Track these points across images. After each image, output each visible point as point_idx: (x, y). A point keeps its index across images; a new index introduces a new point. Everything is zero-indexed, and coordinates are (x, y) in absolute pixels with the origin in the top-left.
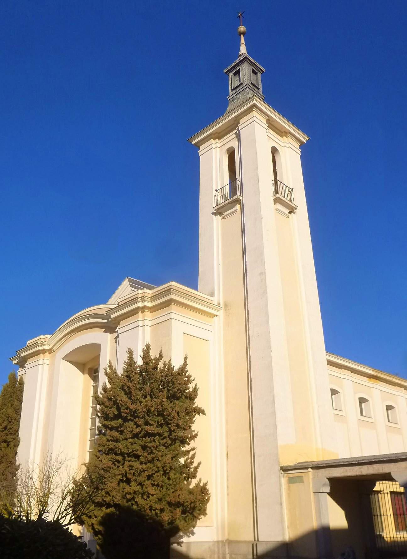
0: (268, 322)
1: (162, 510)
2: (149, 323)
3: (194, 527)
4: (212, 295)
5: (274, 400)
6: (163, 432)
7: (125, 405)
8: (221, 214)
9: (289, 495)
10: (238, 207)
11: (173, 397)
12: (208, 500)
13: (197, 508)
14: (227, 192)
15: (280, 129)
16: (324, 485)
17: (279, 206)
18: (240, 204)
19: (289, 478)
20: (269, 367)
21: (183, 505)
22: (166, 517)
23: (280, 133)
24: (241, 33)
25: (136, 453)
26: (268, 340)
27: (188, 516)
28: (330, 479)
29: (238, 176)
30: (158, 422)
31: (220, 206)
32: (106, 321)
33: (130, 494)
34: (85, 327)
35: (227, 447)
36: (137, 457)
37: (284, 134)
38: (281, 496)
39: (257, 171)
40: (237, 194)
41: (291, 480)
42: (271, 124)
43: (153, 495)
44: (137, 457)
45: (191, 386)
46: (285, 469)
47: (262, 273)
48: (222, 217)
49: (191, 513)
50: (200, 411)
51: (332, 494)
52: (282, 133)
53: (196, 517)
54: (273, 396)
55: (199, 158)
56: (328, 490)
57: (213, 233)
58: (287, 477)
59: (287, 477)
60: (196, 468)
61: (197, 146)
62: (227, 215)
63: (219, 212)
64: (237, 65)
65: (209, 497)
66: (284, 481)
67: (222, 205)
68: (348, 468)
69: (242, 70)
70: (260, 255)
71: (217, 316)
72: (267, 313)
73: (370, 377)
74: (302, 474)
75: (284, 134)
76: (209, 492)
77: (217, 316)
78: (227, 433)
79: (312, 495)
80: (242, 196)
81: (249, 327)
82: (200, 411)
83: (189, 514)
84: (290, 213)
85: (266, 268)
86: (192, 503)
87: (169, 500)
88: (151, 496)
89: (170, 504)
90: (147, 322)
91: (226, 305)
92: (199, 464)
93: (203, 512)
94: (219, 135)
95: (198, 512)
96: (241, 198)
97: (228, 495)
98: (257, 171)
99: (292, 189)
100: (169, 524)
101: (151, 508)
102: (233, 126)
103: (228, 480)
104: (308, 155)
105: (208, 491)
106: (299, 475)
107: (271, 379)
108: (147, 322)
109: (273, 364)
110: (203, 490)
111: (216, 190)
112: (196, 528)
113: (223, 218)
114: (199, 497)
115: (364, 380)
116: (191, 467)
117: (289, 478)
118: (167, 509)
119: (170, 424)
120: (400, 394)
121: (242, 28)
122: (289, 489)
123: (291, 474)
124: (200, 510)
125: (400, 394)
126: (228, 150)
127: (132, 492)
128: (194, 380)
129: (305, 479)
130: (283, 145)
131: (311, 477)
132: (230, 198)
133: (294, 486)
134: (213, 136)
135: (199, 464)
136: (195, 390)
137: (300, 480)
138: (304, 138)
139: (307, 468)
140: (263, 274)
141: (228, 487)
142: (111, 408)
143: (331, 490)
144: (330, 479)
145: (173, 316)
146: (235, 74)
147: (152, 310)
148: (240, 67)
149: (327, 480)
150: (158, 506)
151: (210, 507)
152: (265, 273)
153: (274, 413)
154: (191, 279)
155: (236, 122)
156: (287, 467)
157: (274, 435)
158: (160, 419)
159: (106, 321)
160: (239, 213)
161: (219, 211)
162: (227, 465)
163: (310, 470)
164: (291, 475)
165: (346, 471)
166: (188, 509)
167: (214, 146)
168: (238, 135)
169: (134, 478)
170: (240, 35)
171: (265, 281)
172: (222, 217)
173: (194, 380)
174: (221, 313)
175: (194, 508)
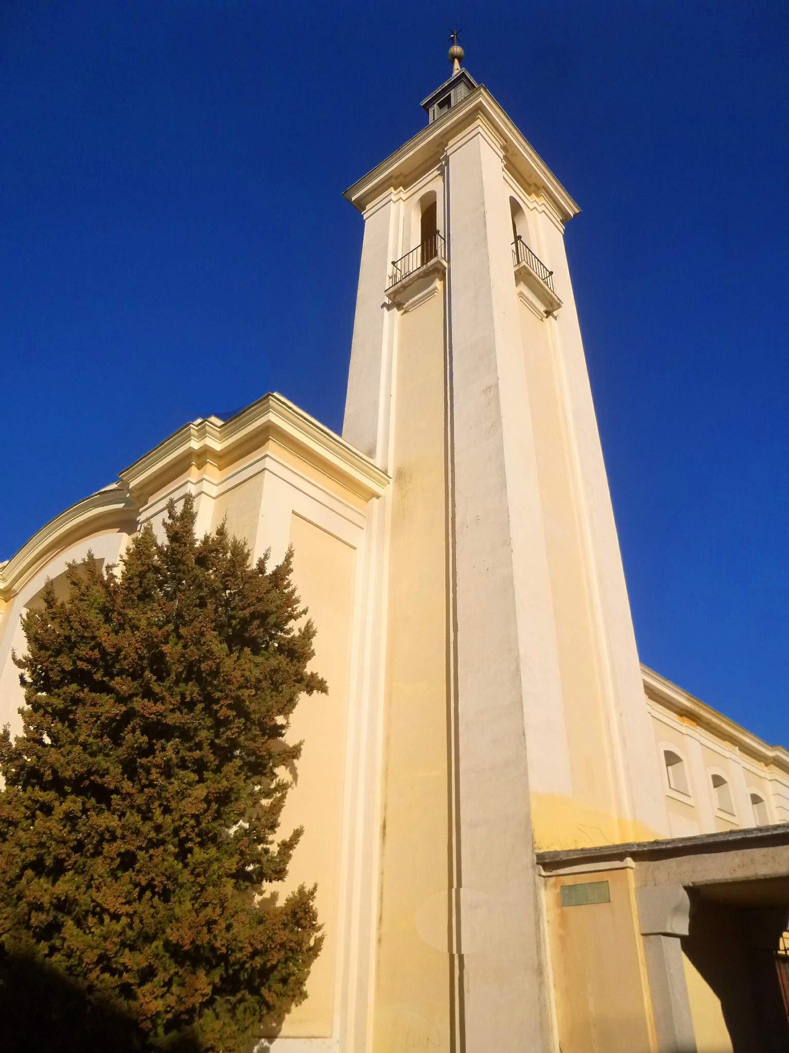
0: (503, 485)
1: (147, 974)
2: (214, 491)
3: (271, 1037)
4: (371, 453)
5: (518, 669)
6: (196, 729)
7: (94, 638)
8: (399, 306)
9: (563, 941)
10: (438, 284)
11: (239, 638)
12: (314, 951)
13: (276, 975)
14: (415, 262)
15: (526, 175)
16: (677, 910)
17: (523, 288)
18: (443, 278)
19: (563, 887)
20: (507, 587)
21: (224, 958)
22: (152, 1001)
23: (527, 186)
24: (454, 57)
25: (99, 780)
26: (505, 526)
27: (241, 1000)
28: (693, 891)
29: (440, 225)
30: (183, 696)
31: (399, 284)
32: (121, 506)
33: (39, 908)
34: (83, 532)
35: (385, 807)
36: (103, 795)
37: (533, 188)
38: (539, 944)
39: (477, 277)
40: (436, 254)
41: (569, 897)
42: (512, 165)
43: (116, 917)
44: (103, 795)
45: (295, 627)
46: (550, 863)
47: (490, 388)
48: (402, 311)
49: (255, 991)
50: (315, 685)
51: (689, 945)
52: (530, 185)
53: (270, 1008)
54: (517, 658)
55: (363, 222)
56: (682, 926)
57: (384, 346)
58: (555, 885)
59: (555, 885)
60: (286, 847)
61: (360, 206)
62: (413, 304)
63: (400, 297)
64: (445, 91)
65: (319, 941)
66: (547, 897)
67: (404, 281)
68: (758, 853)
69: (456, 95)
70: (486, 353)
71: (378, 497)
72: (502, 467)
73: (684, 713)
74: (604, 876)
75: (533, 188)
76: (319, 921)
77: (378, 497)
78: (386, 770)
79: (639, 941)
80: (449, 262)
81: (454, 506)
82: (315, 685)
83: (245, 992)
84: (548, 313)
85: (500, 377)
86: (255, 953)
87: (173, 938)
88: (107, 918)
89: (174, 951)
90: (206, 486)
91: (401, 474)
92: (297, 834)
93: (294, 990)
94: (404, 180)
95: (278, 987)
96: (445, 264)
97: (379, 941)
98: (477, 277)
99: (551, 273)
100: (168, 1027)
101: (105, 962)
102: (436, 159)
103: (381, 899)
104: (576, 236)
105: (314, 917)
106: (595, 878)
107: (511, 618)
108: (206, 486)
109: (516, 582)
110: (301, 913)
111: (394, 263)
112: (277, 1041)
113: (406, 312)
114: (283, 935)
115: (671, 718)
116: (270, 838)
117: (563, 887)
118: (168, 968)
119: (217, 701)
120: (733, 757)
121: (457, 49)
122: (563, 921)
123: (570, 876)
124: (284, 981)
125: (733, 757)
126: (422, 200)
127: (46, 899)
128: (305, 612)
129: (614, 891)
130: (531, 206)
131: (633, 885)
132: (423, 264)
133: (577, 914)
134: (393, 181)
135: (297, 834)
136: (308, 633)
137: (599, 894)
138: (572, 209)
139: (620, 856)
140: (493, 389)
141: (380, 919)
142: (58, 653)
143: (692, 927)
144: (693, 891)
145: (268, 463)
146: (441, 106)
147: (222, 462)
148: (452, 92)
149: (684, 894)
150: (133, 960)
151: (319, 978)
152: (497, 386)
153: (519, 704)
154: (326, 401)
155: (442, 143)
156: (557, 853)
157: (518, 763)
158: (192, 690)
159: (121, 506)
160: (439, 295)
161: (398, 298)
162: (382, 855)
163: (629, 861)
164: (569, 881)
165: (753, 861)
166: (244, 976)
167: (394, 198)
168: (444, 173)
169: (75, 857)
170: (453, 62)
171: (498, 400)
172: (402, 311)
173: (305, 612)
174: (388, 491)
175: (265, 973)
